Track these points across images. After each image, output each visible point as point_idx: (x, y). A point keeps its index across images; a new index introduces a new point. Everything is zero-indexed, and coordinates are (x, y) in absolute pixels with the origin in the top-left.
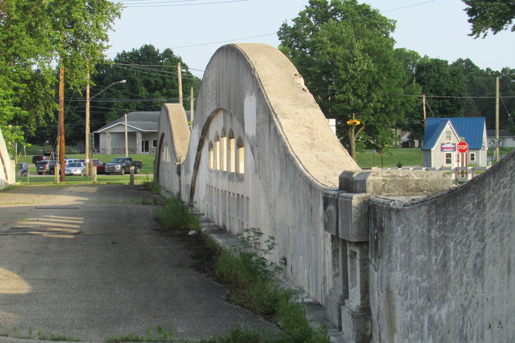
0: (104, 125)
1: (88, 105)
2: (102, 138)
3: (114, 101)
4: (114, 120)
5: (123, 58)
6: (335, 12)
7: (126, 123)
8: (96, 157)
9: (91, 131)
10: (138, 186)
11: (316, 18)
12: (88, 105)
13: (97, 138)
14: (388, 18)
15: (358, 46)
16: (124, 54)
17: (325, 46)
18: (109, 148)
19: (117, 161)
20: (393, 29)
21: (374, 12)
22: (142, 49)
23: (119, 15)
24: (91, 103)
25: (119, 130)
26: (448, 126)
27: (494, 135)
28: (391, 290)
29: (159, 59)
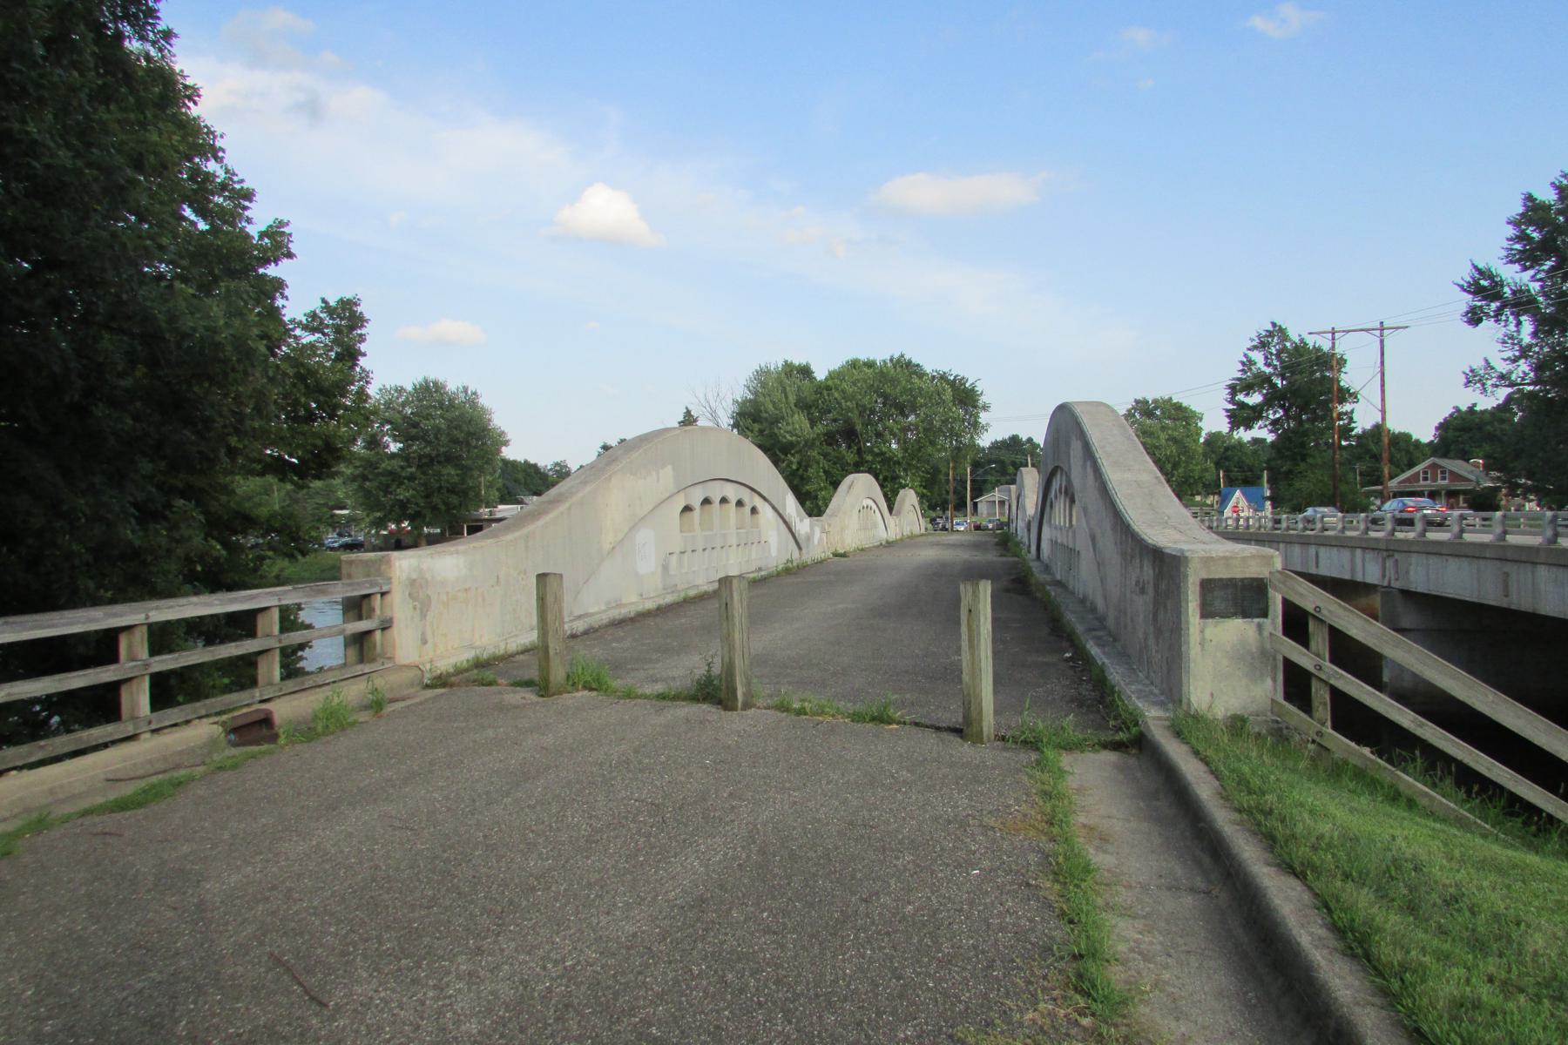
0: (981, 495)
1: (969, 482)
2: (979, 506)
3: (989, 478)
4: (989, 492)
5: (996, 446)
6: (1156, 408)
7: (996, 494)
8: (974, 519)
9: (972, 500)
10: (1181, 690)
11: (1140, 413)
12: (969, 482)
13: (975, 505)
14: (1198, 411)
15: (1163, 436)
16: (996, 442)
17: (1552, 299)
18: (985, 512)
19: (990, 522)
20: (1201, 419)
21: (1186, 408)
22: (1010, 438)
23: (987, 430)
24: (971, 480)
25: (992, 499)
26: (1238, 493)
27: (560, 494)
28: (750, 396)
29: (1023, 445)
